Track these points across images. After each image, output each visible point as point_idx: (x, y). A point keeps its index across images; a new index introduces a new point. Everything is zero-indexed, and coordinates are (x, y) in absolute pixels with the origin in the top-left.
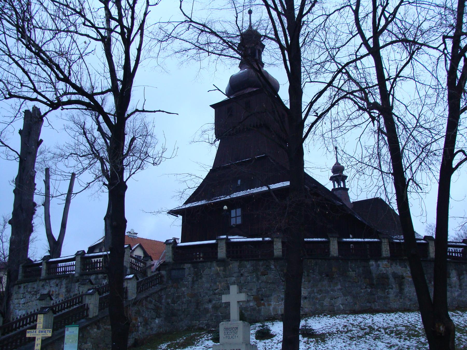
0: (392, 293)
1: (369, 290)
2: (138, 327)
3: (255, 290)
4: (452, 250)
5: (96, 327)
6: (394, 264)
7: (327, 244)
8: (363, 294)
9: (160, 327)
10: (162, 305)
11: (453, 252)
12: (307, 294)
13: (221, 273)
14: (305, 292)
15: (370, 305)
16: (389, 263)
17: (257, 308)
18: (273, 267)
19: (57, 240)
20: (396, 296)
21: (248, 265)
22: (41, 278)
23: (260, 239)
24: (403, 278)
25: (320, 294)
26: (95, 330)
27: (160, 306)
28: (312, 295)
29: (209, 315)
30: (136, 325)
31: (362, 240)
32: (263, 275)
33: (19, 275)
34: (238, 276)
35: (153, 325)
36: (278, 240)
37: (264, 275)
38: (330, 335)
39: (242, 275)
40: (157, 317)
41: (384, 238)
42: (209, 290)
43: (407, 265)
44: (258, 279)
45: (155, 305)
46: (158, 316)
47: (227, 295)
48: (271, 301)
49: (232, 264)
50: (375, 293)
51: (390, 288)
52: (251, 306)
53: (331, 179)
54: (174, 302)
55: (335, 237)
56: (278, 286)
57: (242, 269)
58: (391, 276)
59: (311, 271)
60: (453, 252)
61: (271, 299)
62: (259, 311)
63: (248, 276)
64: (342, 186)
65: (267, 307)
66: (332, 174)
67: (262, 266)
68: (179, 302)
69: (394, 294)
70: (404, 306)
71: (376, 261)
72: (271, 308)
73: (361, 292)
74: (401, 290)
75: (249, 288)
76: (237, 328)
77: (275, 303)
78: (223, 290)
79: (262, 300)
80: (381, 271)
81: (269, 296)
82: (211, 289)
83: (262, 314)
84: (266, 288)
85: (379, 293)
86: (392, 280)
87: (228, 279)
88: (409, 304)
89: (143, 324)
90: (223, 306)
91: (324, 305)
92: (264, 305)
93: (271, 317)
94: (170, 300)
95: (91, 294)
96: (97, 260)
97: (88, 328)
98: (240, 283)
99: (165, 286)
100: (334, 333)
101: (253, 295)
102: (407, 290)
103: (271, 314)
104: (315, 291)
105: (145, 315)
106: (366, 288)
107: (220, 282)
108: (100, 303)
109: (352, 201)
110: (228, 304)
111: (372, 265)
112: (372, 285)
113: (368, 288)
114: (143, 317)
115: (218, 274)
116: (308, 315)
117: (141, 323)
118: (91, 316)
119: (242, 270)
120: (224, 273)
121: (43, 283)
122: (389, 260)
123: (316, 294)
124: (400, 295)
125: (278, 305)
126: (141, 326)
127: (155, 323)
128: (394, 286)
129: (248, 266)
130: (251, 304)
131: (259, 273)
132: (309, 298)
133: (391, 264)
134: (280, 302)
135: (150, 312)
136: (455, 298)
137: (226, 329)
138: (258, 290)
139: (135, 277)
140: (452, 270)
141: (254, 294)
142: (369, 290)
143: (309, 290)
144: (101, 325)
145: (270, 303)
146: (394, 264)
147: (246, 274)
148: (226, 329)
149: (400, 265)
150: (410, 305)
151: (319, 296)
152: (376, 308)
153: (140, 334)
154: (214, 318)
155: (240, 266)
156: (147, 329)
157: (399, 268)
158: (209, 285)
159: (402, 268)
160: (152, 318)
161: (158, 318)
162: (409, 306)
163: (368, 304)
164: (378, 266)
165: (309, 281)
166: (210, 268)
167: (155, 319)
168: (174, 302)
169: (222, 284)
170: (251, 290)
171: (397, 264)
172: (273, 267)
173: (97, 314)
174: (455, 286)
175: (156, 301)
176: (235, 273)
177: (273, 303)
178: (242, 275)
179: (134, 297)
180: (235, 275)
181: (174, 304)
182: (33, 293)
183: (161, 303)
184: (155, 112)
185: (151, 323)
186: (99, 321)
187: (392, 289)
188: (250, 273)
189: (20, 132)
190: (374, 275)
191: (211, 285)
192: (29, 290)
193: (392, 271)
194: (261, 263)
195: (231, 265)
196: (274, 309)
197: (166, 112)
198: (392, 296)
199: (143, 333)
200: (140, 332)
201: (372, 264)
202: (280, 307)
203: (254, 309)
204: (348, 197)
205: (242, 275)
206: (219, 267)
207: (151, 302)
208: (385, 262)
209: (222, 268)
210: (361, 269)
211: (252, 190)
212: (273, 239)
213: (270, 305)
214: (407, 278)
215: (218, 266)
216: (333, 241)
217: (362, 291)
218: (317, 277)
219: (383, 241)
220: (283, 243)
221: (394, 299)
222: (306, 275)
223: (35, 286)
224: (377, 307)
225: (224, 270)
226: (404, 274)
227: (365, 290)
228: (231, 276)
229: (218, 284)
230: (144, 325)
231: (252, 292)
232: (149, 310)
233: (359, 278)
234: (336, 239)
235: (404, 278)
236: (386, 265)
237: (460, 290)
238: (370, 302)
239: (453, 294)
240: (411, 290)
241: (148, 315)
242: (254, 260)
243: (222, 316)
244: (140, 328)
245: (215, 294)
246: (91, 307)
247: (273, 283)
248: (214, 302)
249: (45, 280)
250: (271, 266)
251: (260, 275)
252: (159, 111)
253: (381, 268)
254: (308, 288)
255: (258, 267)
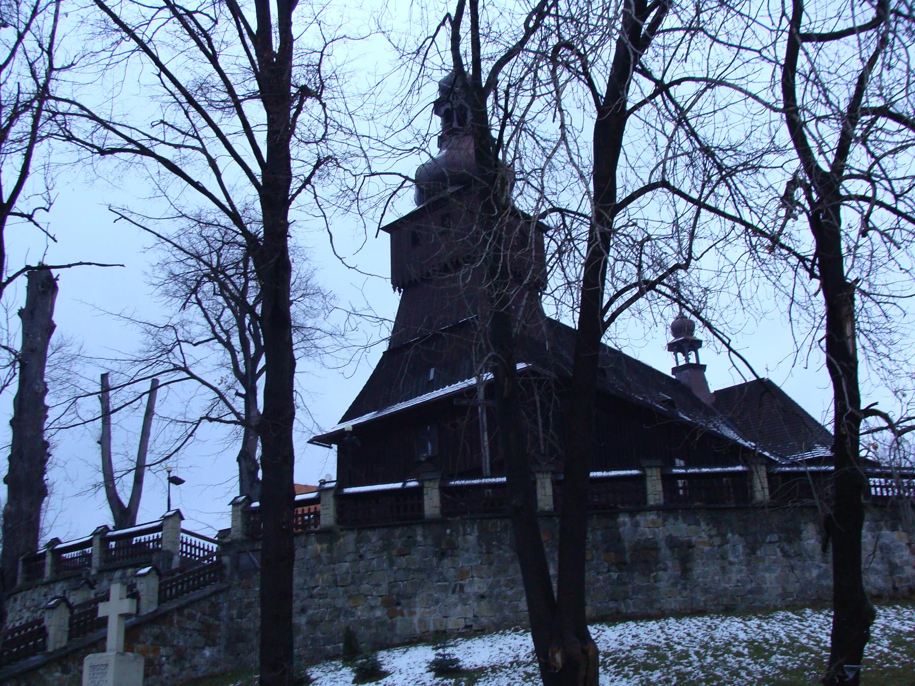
0: (665, 579)
1: (615, 576)
2: (161, 665)
3: (385, 586)
4: (874, 481)
5: (59, 669)
6: (671, 520)
7: (640, 480)
8: (602, 584)
9: (214, 664)
10: (220, 620)
11: (878, 486)
12: (485, 589)
13: (324, 555)
14: (481, 586)
15: (616, 605)
16: (659, 517)
17: (389, 621)
18: (419, 538)
19: (127, 506)
20: (675, 584)
21: (374, 537)
22: (45, 580)
23: (399, 485)
24: (690, 546)
25: (512, 588)
26: (58, 674)
27: (217, 623)
28: (496, 591)
29: (301, 637)
30: (156, 662)
31: (696, 470)
32: (401, 556)
33: (19, 576)
34: (354, 560)
35: (198, 660)
36: (432, 484)
37: (404, 555)
38: (493, 672)
39: (361, 557)
40: (207, 644)
41: (650, 467)
42: (302, 589)
43: (701, 520)
44: (392, 563)
45: (202, 623)
46: (212, 643)
47: (107, 603)
48: (414, 607)
49: (344, 536)
50: (627, 580)
51: (660, 569)
52: (379, 617)
53: (672, 347)
54: (241, 616)
55: (547, 472)
56: (429, 577)
57: (362, 544)
58: (662, 544)
59: (494, 543)
60: (878, 486)
61: (416, 602)
62: (393, 627)
63: (373, 559)
64: (693, 360)
65: (407, 617)
66: (671, 339)
67: (400, 538)
68: (249, 615)
69: (668, 580)
70: (692, 604)
71: (632, 514)
72: (416, 619)
73: (598, 580)
74: (686, 571)
75: (373, 582)
76: (107, 665)
77: (422, 609)
78: (327, 588)
79: (398, 604)
80: (641, 535)
81: (411, 597)
82: (305, 587)
83: (398, 632)
84: (407, 580)
85: (635, 580)
86: (665, 551)
87: (337, 566)
88: (703, 599)
89: (172, 658)
90: (327, 619)
91: (521, 609)
92: (402, 615)
93: (416, 638)
94: (234, 612)
95: (52, 608)
96: (140, 540)
97: (41, 671)
98: (358, 572)
99: (224, 586)
100: (506, 668)
101: (381, 596)
102: (698, 571)
103: (415, 631)
104: (502, 583)
105: (178, 643)
106: (609, 571)
107: (322, 573)
108: (71, 625)
109: (714, 386)
110: (104, 621)
111: (624, 524)
112: (621, 565)
113: (614, 572)
114: (173, 646)
115: (318, 557)
116: (487, 631)
117: (168, 657)
118: (50, 649)
119: (363, 547)
120: (329, 555)
121: (46, 590)
122: (661, 512)
123: (503, 588)
124: (683, 581)
125: (429, 613)
126: (169, 664)
127: (203, 656)
128: (669, 564)
129: (374, 540)
130: (378, 613)
131: (394, 552)
132: (490, 597)
133: (665, 520)
134: (432, 608)
135: (191, 635)
136: (811, 583)
137: (93, 667)
138: (392, 585)
139: (154, 572)
140: (806, 523)
141: (383, 594)
142: (615, 576)
143: (490, 580)
144: (70, 664)
145: (413, 610)
146: (671, 520)
147: (369, 556)
148: (93, 667)
149: (685, 521)
150: (705, 602)
151: (510, 593)
152: (629, 612)
153: (167, 678)
154: (309, 643)
155: (358, 541)
156: (182, 669)
157: (684, 526)
158: (302, 581)
159: (689, 525)
160: (195, 648)
161: (210, 646)
162: (702, 604)
163: (612, 604)
164: (637, 525)
165: (491, 564)
166: (305, 547)
167: (203, 648)
168: (241, 616)
169: (325, 576)
170: (378, 585)
171: (677, 519)
172: (419, 538)
173: (64, 644)
174: (812, 558)
175: (204, 614)
176: (349, 553)
177: (419, 610)
178: (361, 557)
179: (153, 608)
180: (349, 558)
181: (242, 618)
182: (32, 608)
183: (217, 618)
184: (69, 266)
185: (193, 656)
186: (66, 656)
187: (665, 570)
188: (378, 552)
189: (21, 313)
190: (627, 545)
191: (305, 580)
192: (28, 604)
193: (667, 534)
194: (398, 532)
195: (342, 540)
196: (421, 621)
197: (96, 264)
198: (664, 585)
199: (173, 675)
200: (165, 675)
201: (624, 521)
202: (432, 617)
203: (382, 624)
204: (704, 382)
205: (361, 557)
206: (321, 543)
207: (192, 617)
208: (652, 517)
209: (325, 546)
210: (599, 533)
211: (453, 385)
212: (423, 484)
213: (412, 613)
214: (701, 546)
215: (320, 542)
216: (543, 480)
217: (601, 577)
218: (507, 555)
219: (649, 472)
220: (555, 483)
221: (670, 591)
222: (485, 551)
223: (35, 596)
224: (632, 610)
225: (330, 550)
226: (694, 539)
227: (607, 575)
228: (342, 560)
229: (317, 576)
230: (175, 661)
231: (380, 589)
232: (188, 632)
233: (594, 552)
234: (549, 476)
235: (694, 546)
236: (653, 522)
237: (823, 565)
238: (616, 600)
239: (807, 574)
240: (708, 571)
241: (186, 642)
242: (383, 527)
243: (323, 639)
244: (166, 667)
245: (312, 596)
246: (51, 631)
247: (420, 570)
248: (310, 612)
249: (47, 584)
250: (416, 537)
251: (397, 556)
252: (81, 263)
253: (642, 528)
254: (488, 578)
255: (393, 540)
